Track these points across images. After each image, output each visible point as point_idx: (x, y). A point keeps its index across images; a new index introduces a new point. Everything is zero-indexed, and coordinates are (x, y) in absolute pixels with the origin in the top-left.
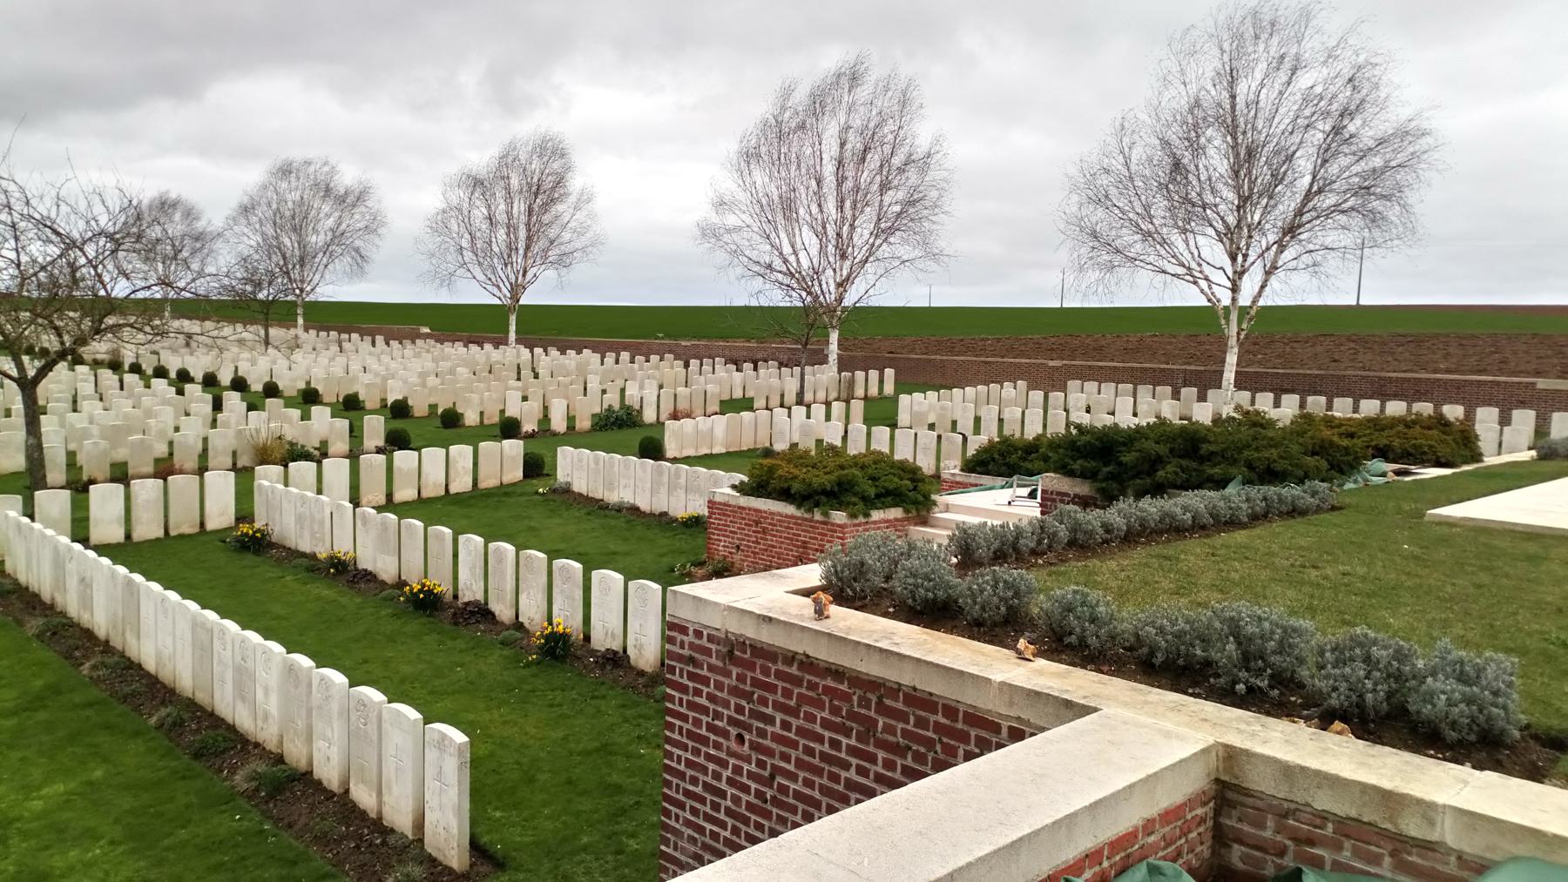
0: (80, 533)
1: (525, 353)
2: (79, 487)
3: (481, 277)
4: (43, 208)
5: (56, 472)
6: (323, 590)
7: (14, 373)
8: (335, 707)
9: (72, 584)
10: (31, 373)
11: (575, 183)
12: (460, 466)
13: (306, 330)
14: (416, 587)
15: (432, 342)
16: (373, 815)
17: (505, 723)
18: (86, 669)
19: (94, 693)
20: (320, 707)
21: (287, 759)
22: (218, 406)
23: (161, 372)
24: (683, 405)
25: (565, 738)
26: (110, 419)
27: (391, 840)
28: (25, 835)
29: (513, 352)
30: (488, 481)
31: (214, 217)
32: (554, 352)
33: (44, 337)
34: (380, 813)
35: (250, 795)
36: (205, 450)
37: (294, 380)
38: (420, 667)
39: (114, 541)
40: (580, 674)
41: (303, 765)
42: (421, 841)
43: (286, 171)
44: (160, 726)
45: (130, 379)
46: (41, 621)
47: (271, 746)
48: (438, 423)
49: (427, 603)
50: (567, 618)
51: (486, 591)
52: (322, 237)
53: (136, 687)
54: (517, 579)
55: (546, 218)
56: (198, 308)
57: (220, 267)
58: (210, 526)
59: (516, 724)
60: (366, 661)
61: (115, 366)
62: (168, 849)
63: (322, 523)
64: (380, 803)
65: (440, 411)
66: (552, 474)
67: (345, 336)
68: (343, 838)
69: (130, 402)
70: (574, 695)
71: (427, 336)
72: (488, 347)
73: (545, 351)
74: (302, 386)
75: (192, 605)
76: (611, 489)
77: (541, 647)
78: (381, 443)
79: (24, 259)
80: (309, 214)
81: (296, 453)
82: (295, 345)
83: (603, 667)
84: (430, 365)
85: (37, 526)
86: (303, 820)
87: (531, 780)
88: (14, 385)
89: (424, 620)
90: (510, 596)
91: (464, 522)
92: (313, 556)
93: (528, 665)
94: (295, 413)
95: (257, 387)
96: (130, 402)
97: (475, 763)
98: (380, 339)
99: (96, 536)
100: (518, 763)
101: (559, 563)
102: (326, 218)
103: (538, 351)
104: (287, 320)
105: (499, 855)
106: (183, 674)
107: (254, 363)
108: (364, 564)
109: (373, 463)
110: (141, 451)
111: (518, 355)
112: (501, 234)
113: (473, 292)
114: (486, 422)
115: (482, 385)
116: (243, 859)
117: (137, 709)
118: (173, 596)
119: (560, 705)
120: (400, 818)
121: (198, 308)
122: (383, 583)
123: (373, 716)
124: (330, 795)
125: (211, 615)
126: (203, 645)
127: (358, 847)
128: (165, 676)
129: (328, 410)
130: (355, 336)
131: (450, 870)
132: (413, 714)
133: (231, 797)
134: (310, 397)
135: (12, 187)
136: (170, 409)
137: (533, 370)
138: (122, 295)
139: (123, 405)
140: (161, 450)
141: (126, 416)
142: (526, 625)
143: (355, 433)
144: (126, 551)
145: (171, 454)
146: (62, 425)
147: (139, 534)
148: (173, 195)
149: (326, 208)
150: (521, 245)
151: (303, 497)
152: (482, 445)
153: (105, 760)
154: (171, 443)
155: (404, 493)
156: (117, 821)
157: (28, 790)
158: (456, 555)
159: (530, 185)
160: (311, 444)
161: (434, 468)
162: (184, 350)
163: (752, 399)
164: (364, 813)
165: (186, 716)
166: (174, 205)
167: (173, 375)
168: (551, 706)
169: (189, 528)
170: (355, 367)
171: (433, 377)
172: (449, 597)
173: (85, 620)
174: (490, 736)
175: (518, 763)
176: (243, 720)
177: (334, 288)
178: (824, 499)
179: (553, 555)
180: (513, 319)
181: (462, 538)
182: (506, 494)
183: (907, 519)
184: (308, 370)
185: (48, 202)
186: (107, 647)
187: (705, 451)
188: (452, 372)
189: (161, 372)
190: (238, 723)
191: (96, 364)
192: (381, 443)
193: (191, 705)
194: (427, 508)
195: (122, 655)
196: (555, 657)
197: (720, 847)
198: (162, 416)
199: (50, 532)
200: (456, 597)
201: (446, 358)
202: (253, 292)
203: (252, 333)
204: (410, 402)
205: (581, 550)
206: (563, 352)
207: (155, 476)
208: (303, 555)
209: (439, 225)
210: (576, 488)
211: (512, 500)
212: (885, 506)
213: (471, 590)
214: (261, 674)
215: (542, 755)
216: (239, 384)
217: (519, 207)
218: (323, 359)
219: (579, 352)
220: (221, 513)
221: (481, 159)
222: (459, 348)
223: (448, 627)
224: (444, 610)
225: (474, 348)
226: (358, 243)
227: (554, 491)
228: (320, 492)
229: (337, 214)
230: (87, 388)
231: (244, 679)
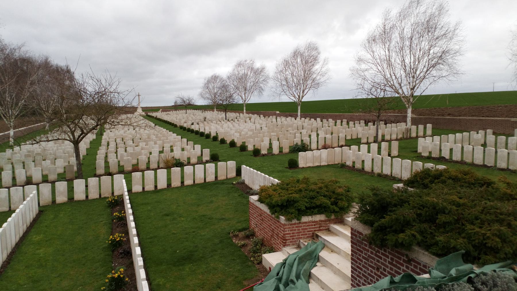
11: (322, 57)
12: (210, 171)
24: (328, 142)
30: (221, 177)
36: (149, 161)
39: (95, 198)
69: (145, 143)
145: (65, 172)
148: (217, 75)
163: (360, 138)
178: (278, 209)
183: (329, 221)
187: (317, 164)
197: (386, 273)
212: (312, 214)
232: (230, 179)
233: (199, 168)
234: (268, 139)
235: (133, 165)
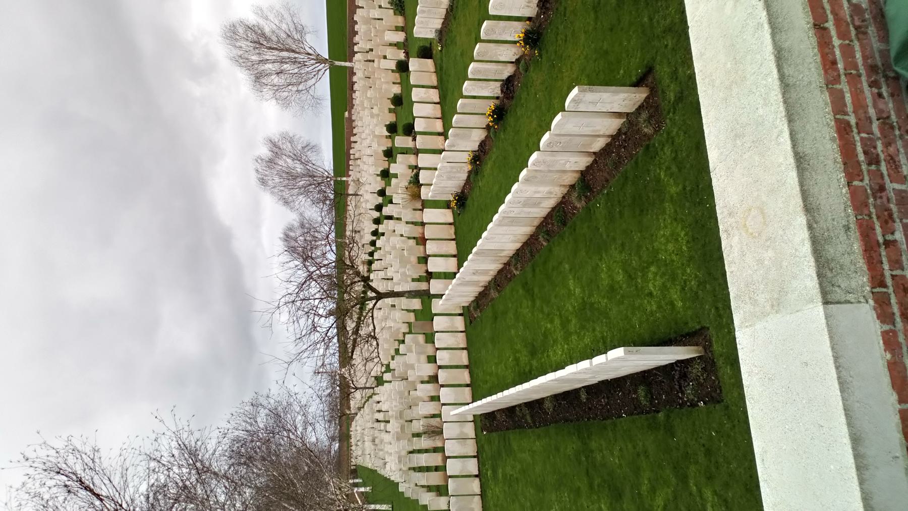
0: (452, 275)
1: (358, 57)
2: (430, 276)
3: (313, 81)
4: (292, 288)
5: (423, 286)
6: (488, 167)
7: (374, 302)
8: (549, 158)
9: (475, 278)
10: (374, 295)
11: (252, 19)
12: (423, 95)
13: (349, 176)
14: (490, 119)
15: (353, 111)
16: (609, 140)
17: (571, 69)
18: (517, 273)
19: (528, 269)
20: (548, 166)
21: (573, 183)
22: (390, 218)
23: (373, 243)
25: (585, 32)
26: (396, 265)
27: (624, 130)
28: (591, 295)
29: (358, 63)
30: (434, 80)
31: (292, 218)
32: (357, 39)
33: (357, 288)
34: (609, 136)
35: (588, 199)
36: (412, 223)
37: (376, 182)
38: (534, 116)
39: (465, 338)
40: (550, 23)
41: (577, 175)
42: (628, 114)
43: (263, 182)
44: (548, 241)
45: (376, 256)
46: (492, 291)
47: (565, 190)
48: (399, 108)
49: (499, 114)
50: (515, 32)
51: (496, 80)
52: (297, 165)
53: (528, 251)
54: (491, 62)
55: (274, 38)
56: (340, 224)
57: (317, 214)
58: (451, 220)
59: (573, 63)
60: (527, 145)
61: (370, 263)
62: (608, 236)
63: (452, 168)
64: (603, 136)
65: (393, 107)
66: (431, 41)
67: (352, 157)
68: (618, 155)
69: (388, 256)
70: (561, 27)
71: (350, 113)
72: (355, 79)
73: (356, 44)
74: (379, 178)
75: (490, 226)
76: (441, 3)
77: (531, 48)
78: (410, 138)
79: (318, 296)
80: (283, 169)
81: (416, 182)
82: (358, 182)
83: (547, 9)
84: (367, 112)
85: (447, 292)
86: (606, 175)
87: (606, 52)
88: (380, 302)
89: (508, 115)
90: (500, 67)
91: (456, 94)
92: (470, 172)
93: (540, 55)
94: (394, 181)
95: (380, 200)
96: (388, 256)
97: (591, 83)
98: (353, 139)
99: (455, 270)
100: (595, 61)
101: (483, 35)
102: (286, 162)
103: (356, 49)
104: (345, 185)
105: (644, 70)
106: (524, 231)
107: (367, 201)
108: (475, 146)
109: (421, 142)
110: (414, 251)
111: (359, 61)
112: (285, 66)
113: (323, 86)
114: (399, 81)
115: (378, 82)
116: (619, 202)
117: (538, 251)
118: (484, 235)
119: (566, 37)
120: (612, 126)
121: (340, 224)
122: (486, 137)
123: (557, 139)
124: (595, 162)
125: (496, 217)
126: (511, 221)
127: (624, 147)
128: (524, 239)
129: (392, 165)
130: (352, 152)
131: (647, 98)
132: (559, 117)
133: (588, 209)
134: (385, 174)
135: (283, 300)
136: (392, 239)
137: (367, 52)
138: (334, 256)
139: (389, 259)
140: (412, 242)
141: (395, 257)
142: (517, 57)
143: (405, 151)
144: (461, 257)
145: (414, 238)
146: (399, 284)
147: (454, 252)
149: (281, 162)
150: (292, 55)
151: (438, 176)
152: (412, 82)
153: (561, 263)
154: (409, 238)
155: (439, 126)
156: (590, 258)
157: (570, 294)
158: (474, 97)
159: (255, 48)
160: (410, 173)
161: (424, 109)
162: (362, 233)
164: (607, 145)
165: (545, 229)
166: (287, 236)
167: (374, 238)
168: (566, 41)
169: (452, 230)
170: (369, 151)
171: (374, 111)
172: (497, 102)
173: (493, 273)
174: (577, 78)
175: (595, 61)
176: (550, 203)
177: (325, 161)
179: (478, 39)
180: (337, 63)
181: (465, 93)
182: (441, 69)
184: (371, 175)
185: (290, 286)
186: (507, 264)
188: (370, 99)
189: (373, 243)
190: (552, 206)
191: (369, 271)
192: (410, 138)
193: (539, 227)
194: (446, 118)
195: (511, 257)
196: (538, 39)
198: (395, 244)
199: (450, 287)
200: (498, 98)
201: (362, 102)
202: (330, 200)
203: (352, 202)
204: (388, 123)
205: (476, 23)
206: (356, 33)
207: (425, 245)
208: (469, 177)
209: (285, 103)
210: (439, 26)
211: (444, 66)
213: (494, 89)
214: (527, 195)
215: (593, 46)
216: (379, 208)
217: (270, 55)
218: (365, 167)
219: (356, 23)
220: (446, 216)
221: (242, 78)
222: (356, 95)
223: (514, 102)
224: (504, 105)
225: (356, 87)
226: (299, 148)
227: (440, 40)
228: (436, 169)
229: (284, 157)
230: (381, 274)
231: (529, 203)
232: (436, 68)
233: (441, 340)
234: (412, 473)
235: (426, 342)
